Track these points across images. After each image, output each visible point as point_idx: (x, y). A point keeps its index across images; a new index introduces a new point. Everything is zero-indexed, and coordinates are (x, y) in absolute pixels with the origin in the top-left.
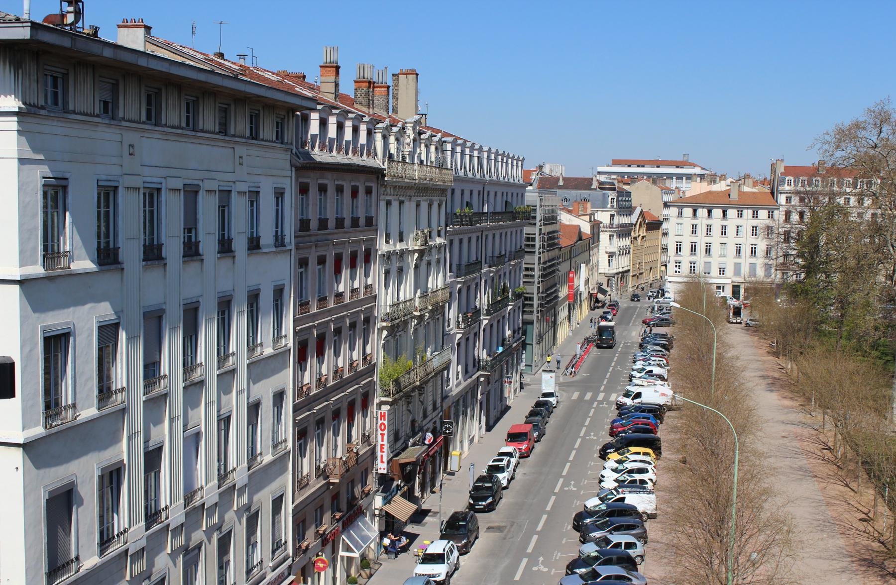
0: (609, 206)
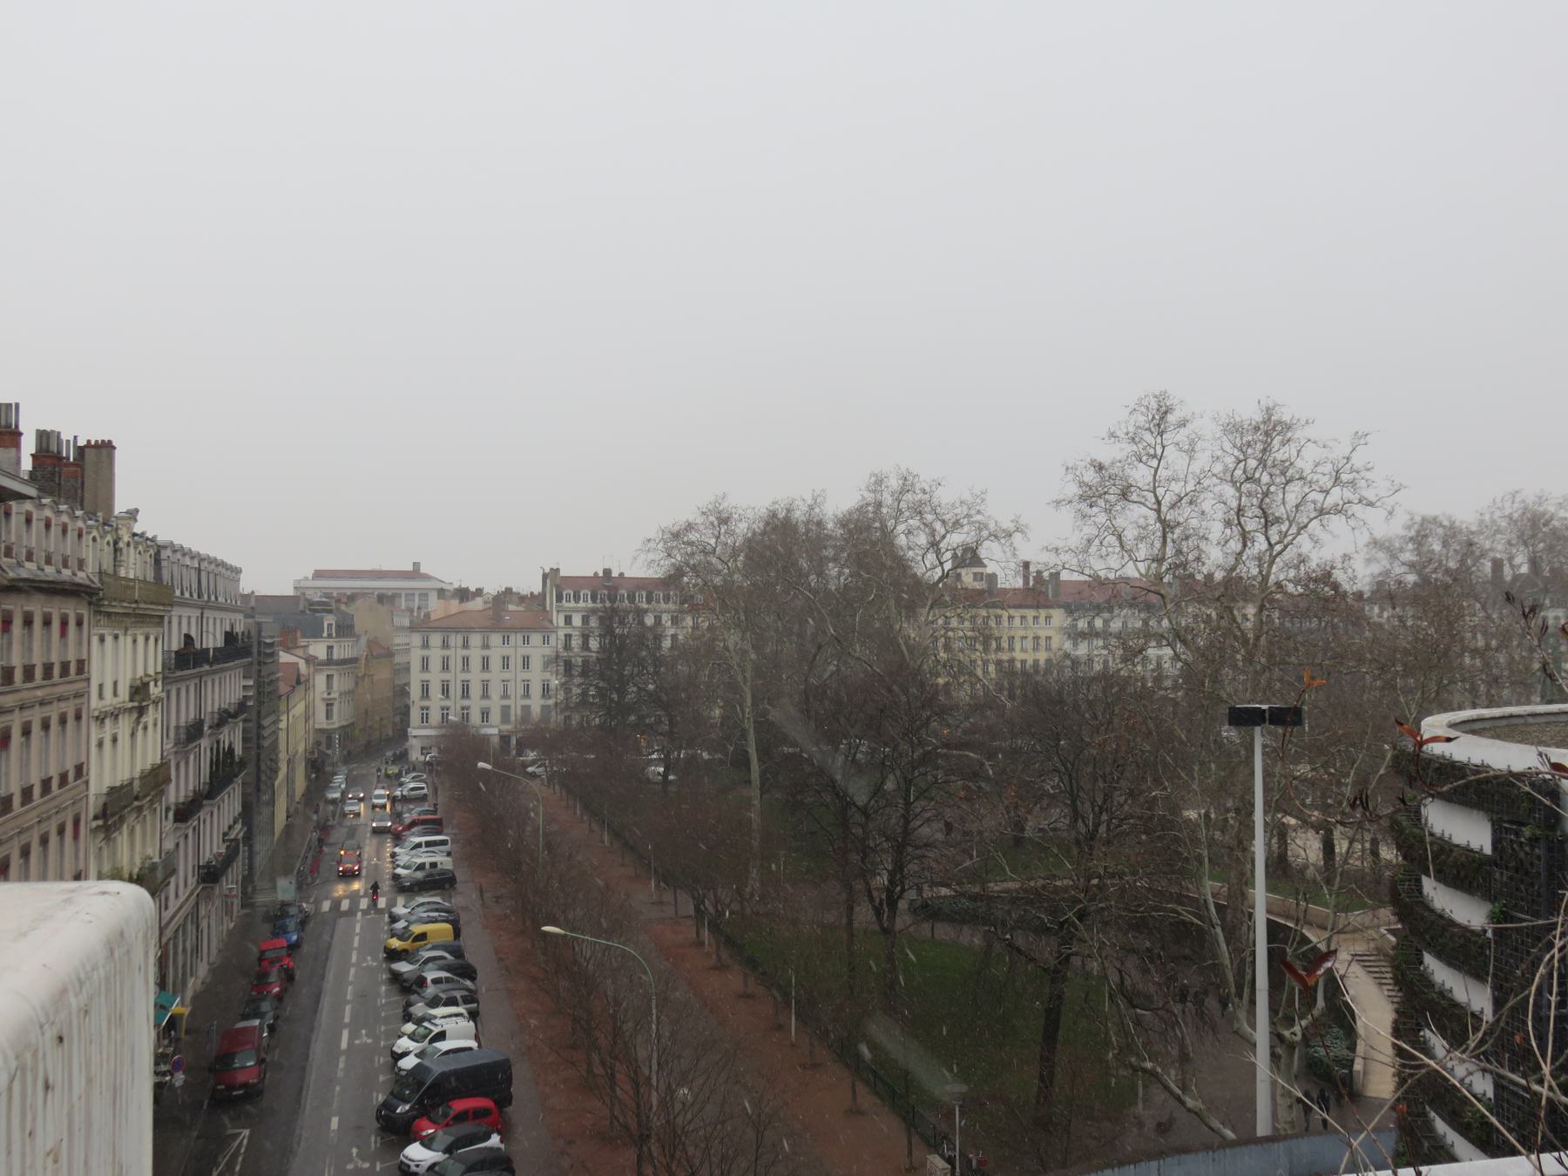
0: (325, 634)
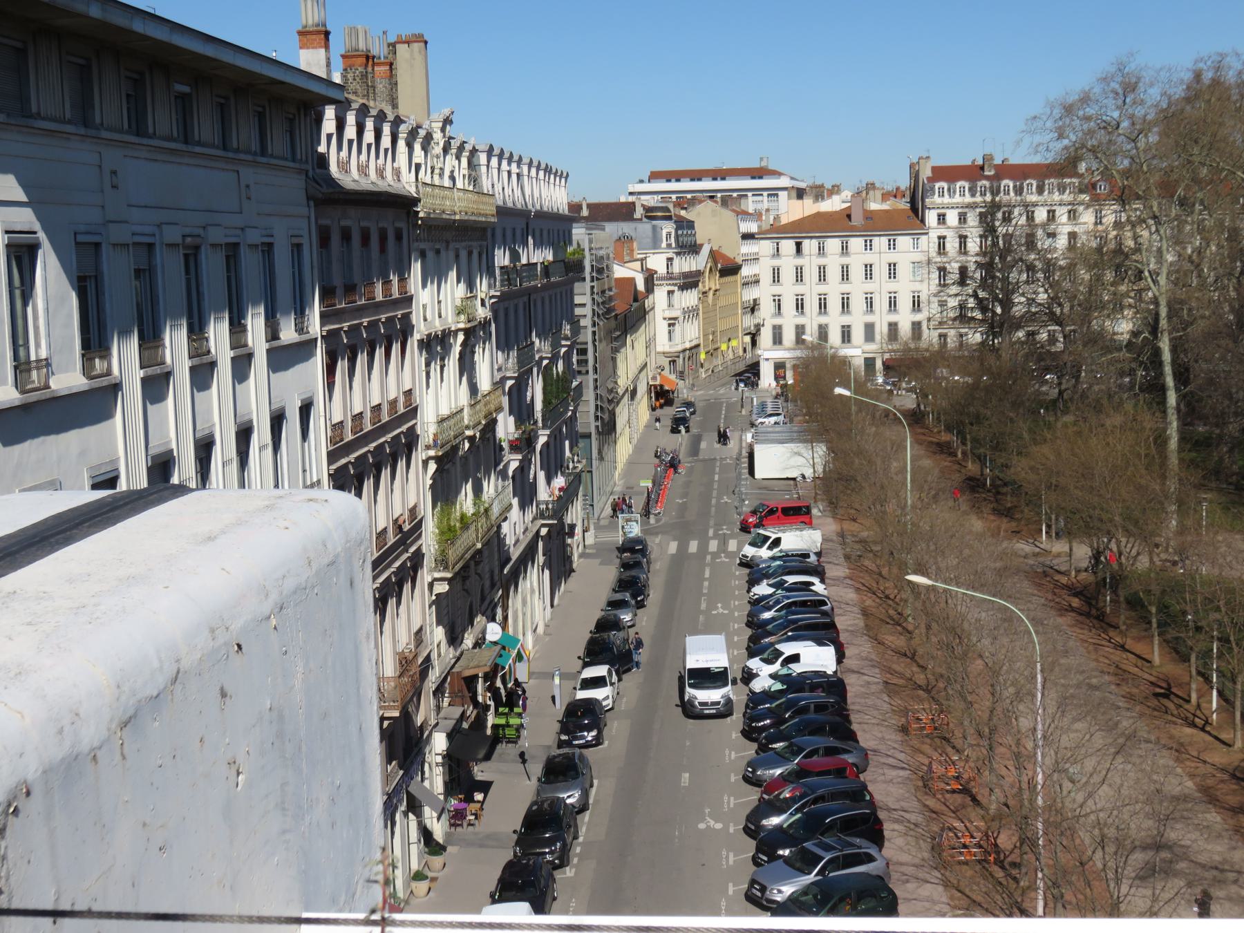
0: (664, 245)
